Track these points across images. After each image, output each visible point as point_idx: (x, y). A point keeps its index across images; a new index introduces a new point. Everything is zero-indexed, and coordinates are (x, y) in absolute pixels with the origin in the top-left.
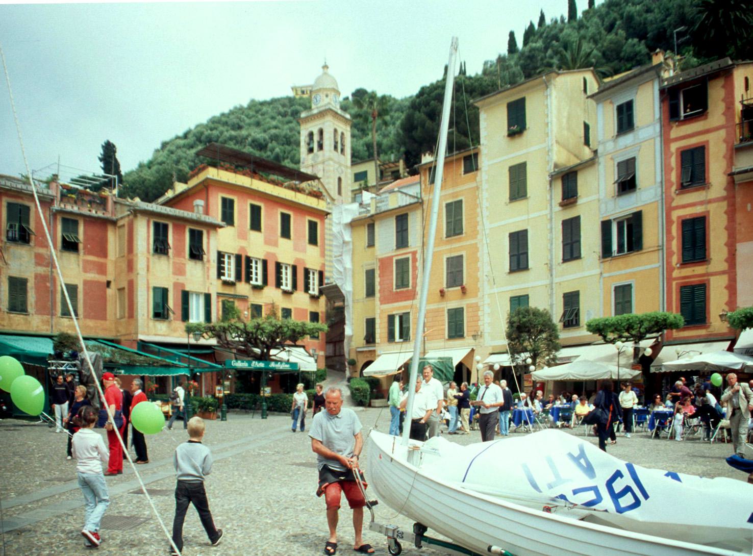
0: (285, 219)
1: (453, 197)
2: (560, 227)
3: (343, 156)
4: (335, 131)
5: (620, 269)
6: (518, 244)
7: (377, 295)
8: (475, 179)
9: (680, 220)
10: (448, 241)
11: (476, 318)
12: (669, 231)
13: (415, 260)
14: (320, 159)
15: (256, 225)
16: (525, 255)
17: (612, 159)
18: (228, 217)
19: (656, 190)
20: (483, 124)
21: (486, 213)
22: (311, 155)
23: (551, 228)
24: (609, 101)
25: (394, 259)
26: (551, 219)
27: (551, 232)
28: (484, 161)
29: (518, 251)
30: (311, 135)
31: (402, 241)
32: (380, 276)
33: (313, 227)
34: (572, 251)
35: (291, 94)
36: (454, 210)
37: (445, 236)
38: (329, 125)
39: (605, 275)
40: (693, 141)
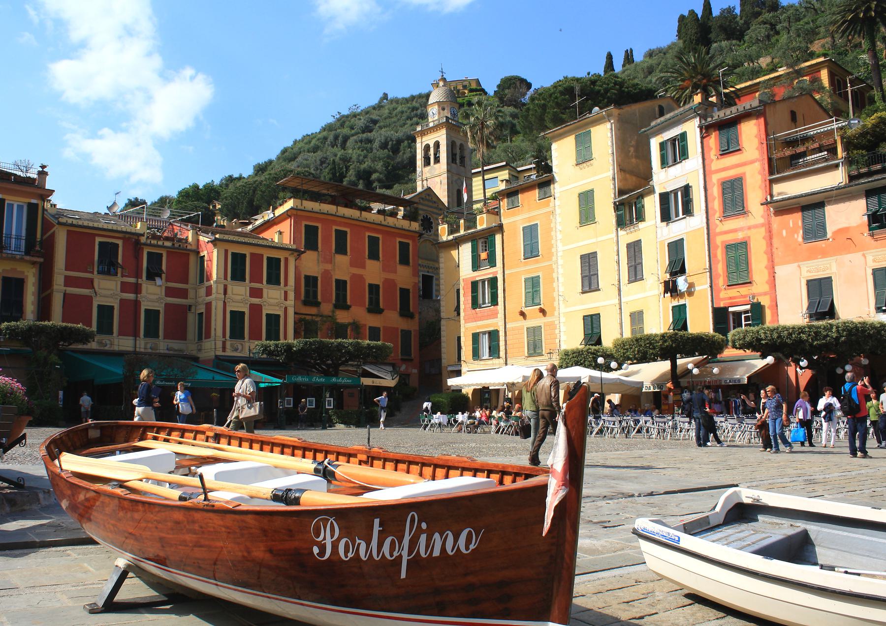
3: (462, 168)
6: (589, 265)
8: (548, 205)
9: (724, 245)
15: (341, 249)
16: (596, 276)
21: (559, 236)
22: (427, 168)
29: (590, 272)
30: (427, 148)
34: (636, 273)
36: (531, 232)
37: (523, 257)
40: (731, 173)
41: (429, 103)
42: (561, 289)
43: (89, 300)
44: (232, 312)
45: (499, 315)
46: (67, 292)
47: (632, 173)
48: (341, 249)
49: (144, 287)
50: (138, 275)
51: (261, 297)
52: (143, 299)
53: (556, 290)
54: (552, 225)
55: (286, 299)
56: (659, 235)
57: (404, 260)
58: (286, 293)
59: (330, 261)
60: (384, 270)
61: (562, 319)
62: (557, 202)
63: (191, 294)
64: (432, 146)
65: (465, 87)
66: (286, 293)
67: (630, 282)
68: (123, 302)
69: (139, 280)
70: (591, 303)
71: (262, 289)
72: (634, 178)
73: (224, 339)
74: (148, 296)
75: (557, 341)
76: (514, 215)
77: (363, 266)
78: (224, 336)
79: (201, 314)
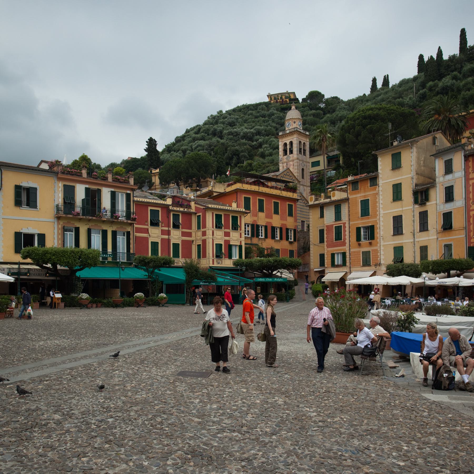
0: (276, 205)
1: (365, 198)
2: (418, 215)
3: (304, 156)
4: (300, 142)
5: (446, 237)
6: (398, 222)
7: (325, 243)
10: (361, 219)
11: (377, 256)
12: (469, 221)
13: (345, 227)
14: (291, 159)
17: (442, 185)
18: (247, 206)
19: (463, 201)
20: (379, 163)
21: (381, 206)
22: (285, 157)
23: (414, 215)
24: (441, 158)
25: (334, 226)
26: (414, 211)
27: (414, 217)
28: (381, 182)
29: (398, 225)
30: (285, 144)
31: (338, 217)
32: (326, 234)
33: (290, 207)
34: (424, 227)
35: (267, 100)
36: (365, 204)
37: (360, 216)
38: (295, 139)
39: (440, 239)
41: (286, 119)
42: (382, 233)
43: (147, 239)
44: (216, 244)
45: (346, 245)
46: (137, 236)
47: (421, 175)
48: (261, 209)
49: (172, 231)
50: (169, 226)
51: (229, 236)
52: (172, 238)
53: (379, 233)
54: (377, 200)
55: (241, 237)
56: (438, 209)
57: (290, 214)
58: (241, 234)
59: (256, 215)
60: (281, 219)
61: (382, 248)
62: (380, 189)
63: (193, 234)
64: (288, 143)
65: (286, 98)
66: (241, 234)
67: (421, 231)
68: (162, 240)
69: (170, 228)
70: (398, 241)
71: (229, 232)
72: (422, 178)
73: (213, 258)
74: (174, 236)
75: (379, 259)
76: (355, 194)
77: (272, 218)
78: (213, 257)
79: (199, 246)
